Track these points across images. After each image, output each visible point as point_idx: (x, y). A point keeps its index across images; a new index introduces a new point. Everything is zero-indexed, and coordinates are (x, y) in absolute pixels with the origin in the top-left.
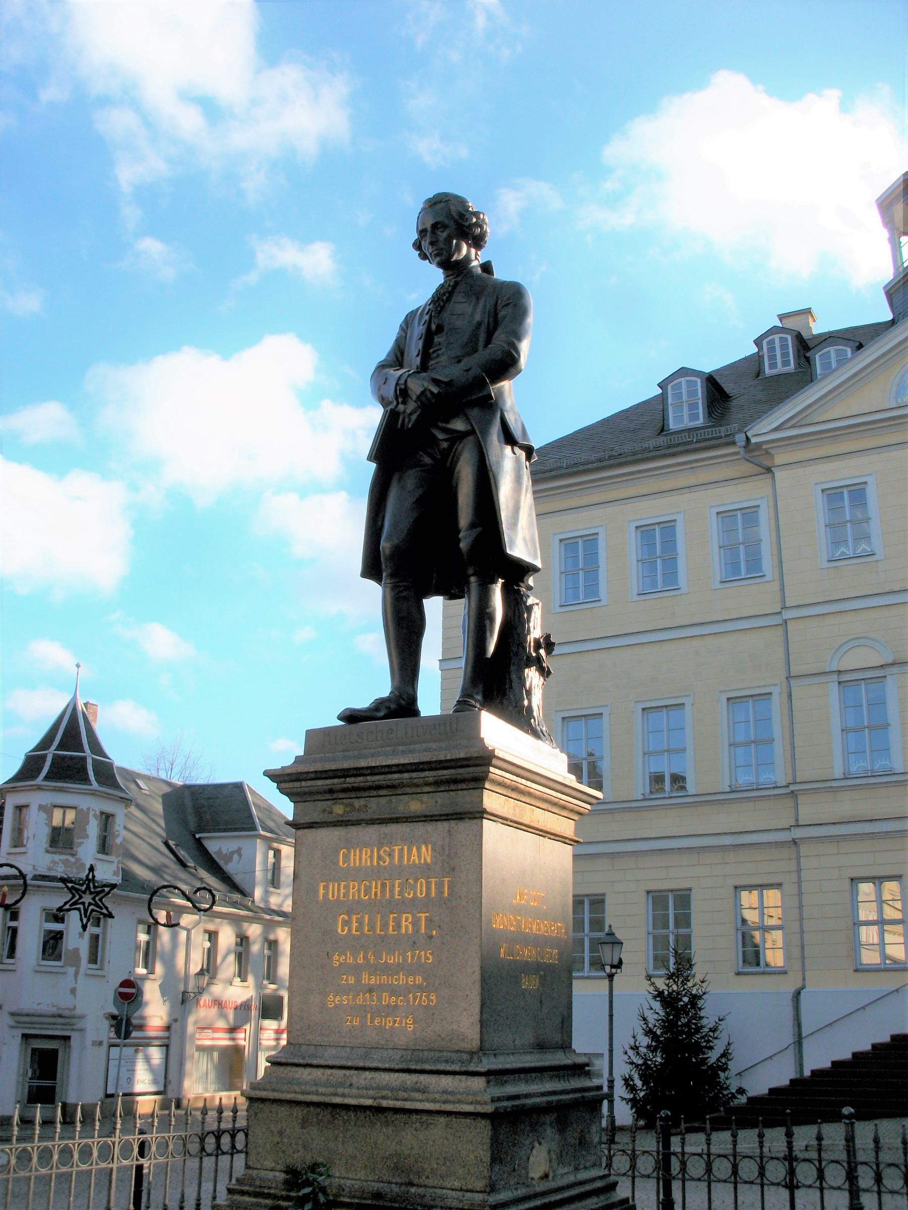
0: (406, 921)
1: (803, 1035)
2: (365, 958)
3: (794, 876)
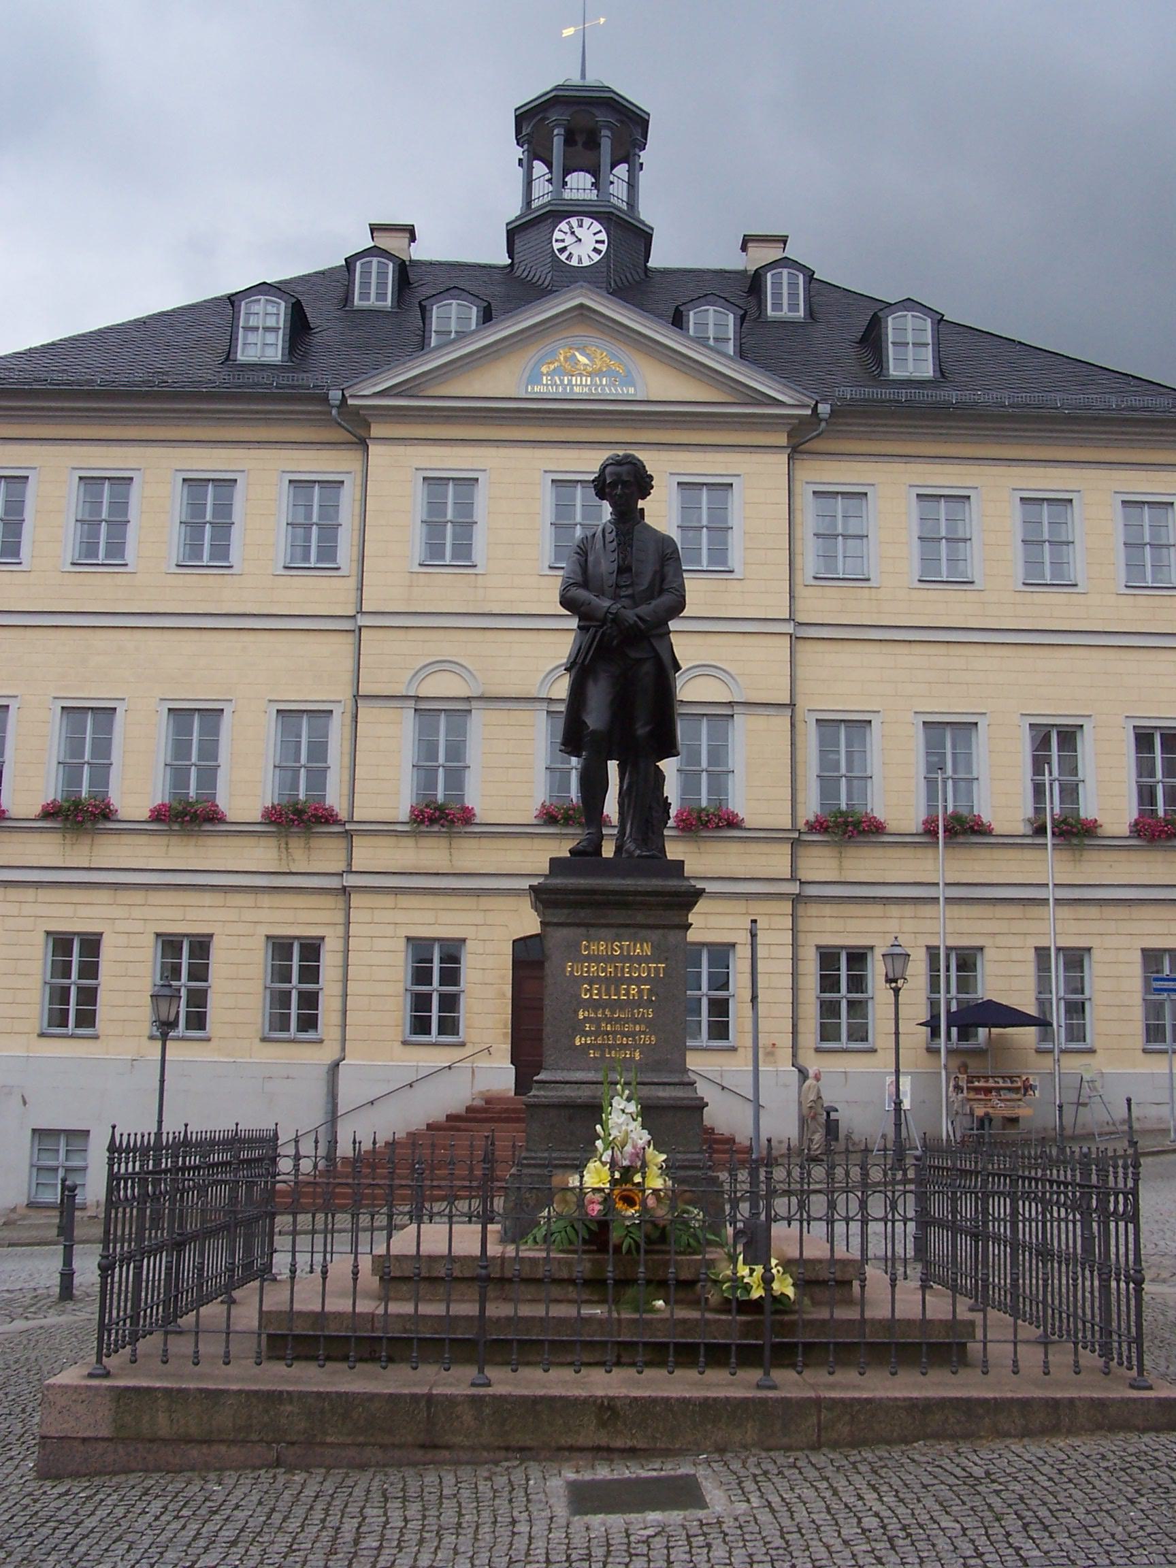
0: (634, 989)
2: (603, 1013)
3: (340, 930)
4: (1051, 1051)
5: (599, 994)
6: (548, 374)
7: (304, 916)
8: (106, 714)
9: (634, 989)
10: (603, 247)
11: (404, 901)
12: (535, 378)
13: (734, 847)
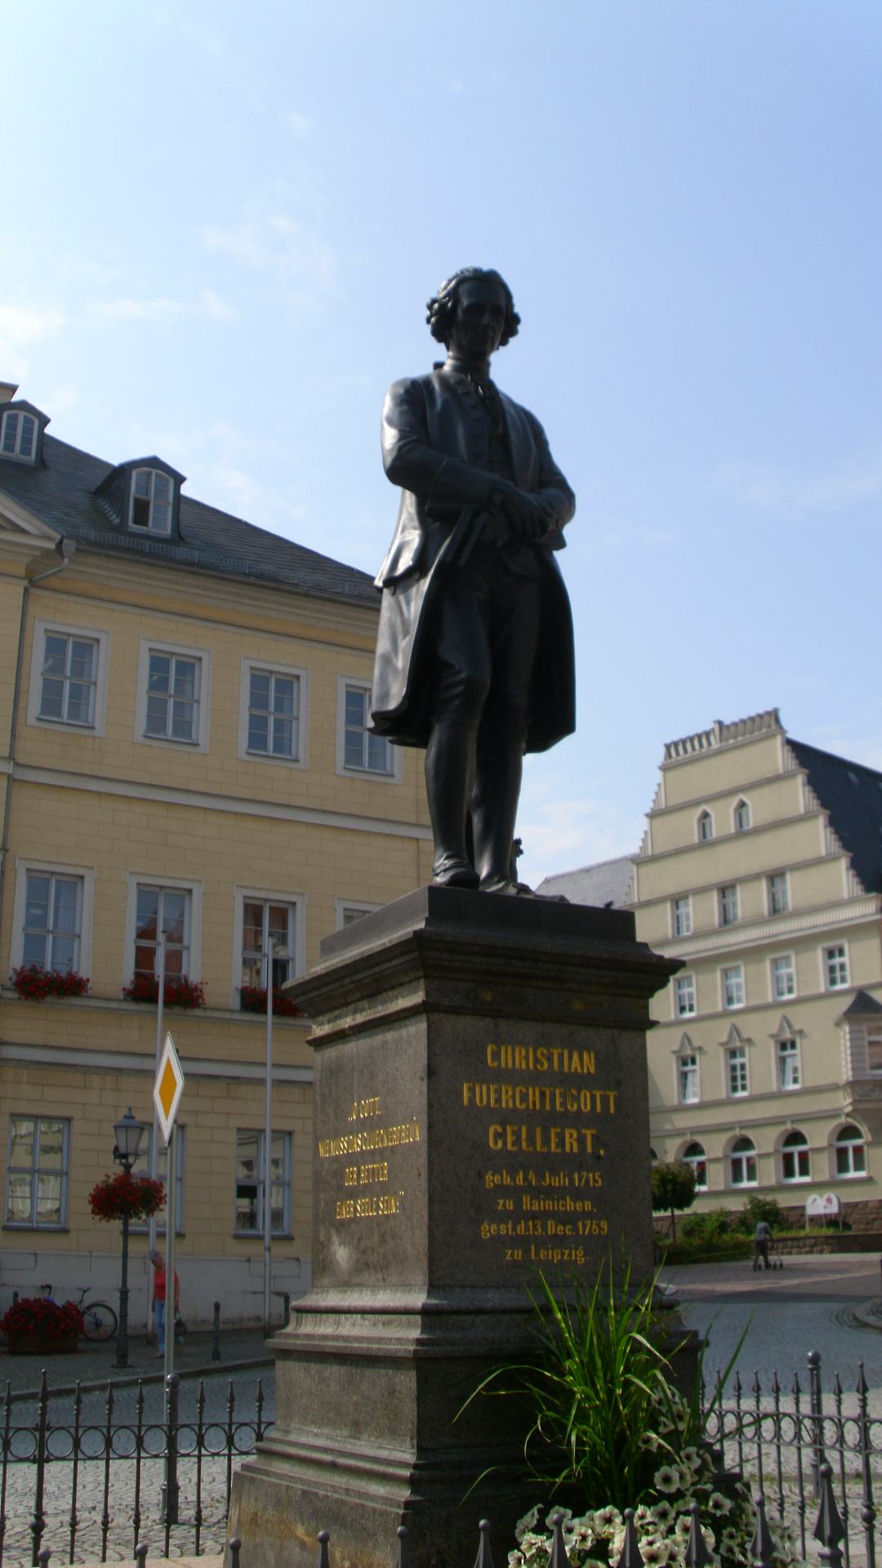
2: (525, 1179)
5: (517, 1142)
9: (571, 1136)
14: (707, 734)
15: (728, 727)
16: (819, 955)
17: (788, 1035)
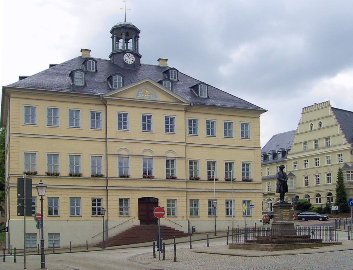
1: (109, 229)
3: (106, 197)
4: (232, 217)
6: (141, 94)
7: (99, 194)
8: (56, 156)
10: (134, 60)
11: (119, 192)
12: (138, 95)
13: (176, 183)
14: (313, 106)
15: (318, 104)
16: (337, 156)
17: (328, 173)
